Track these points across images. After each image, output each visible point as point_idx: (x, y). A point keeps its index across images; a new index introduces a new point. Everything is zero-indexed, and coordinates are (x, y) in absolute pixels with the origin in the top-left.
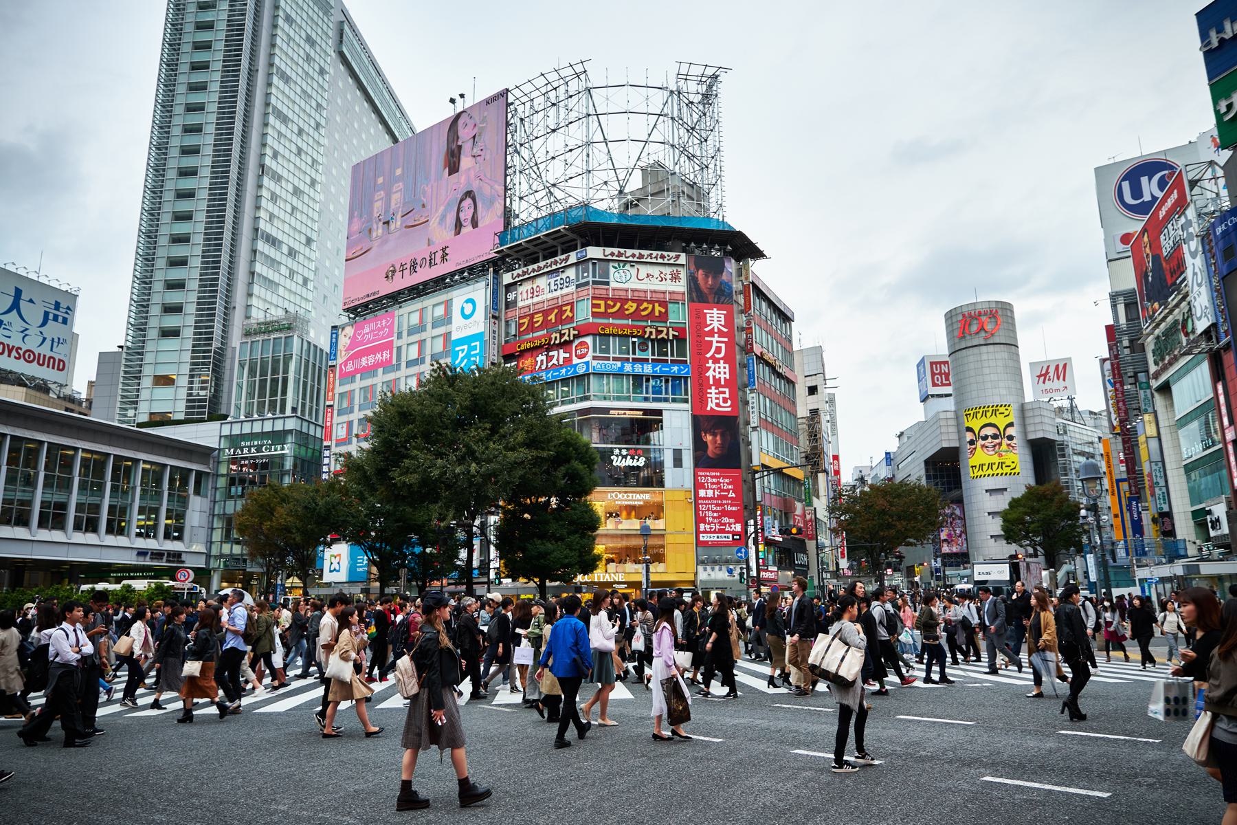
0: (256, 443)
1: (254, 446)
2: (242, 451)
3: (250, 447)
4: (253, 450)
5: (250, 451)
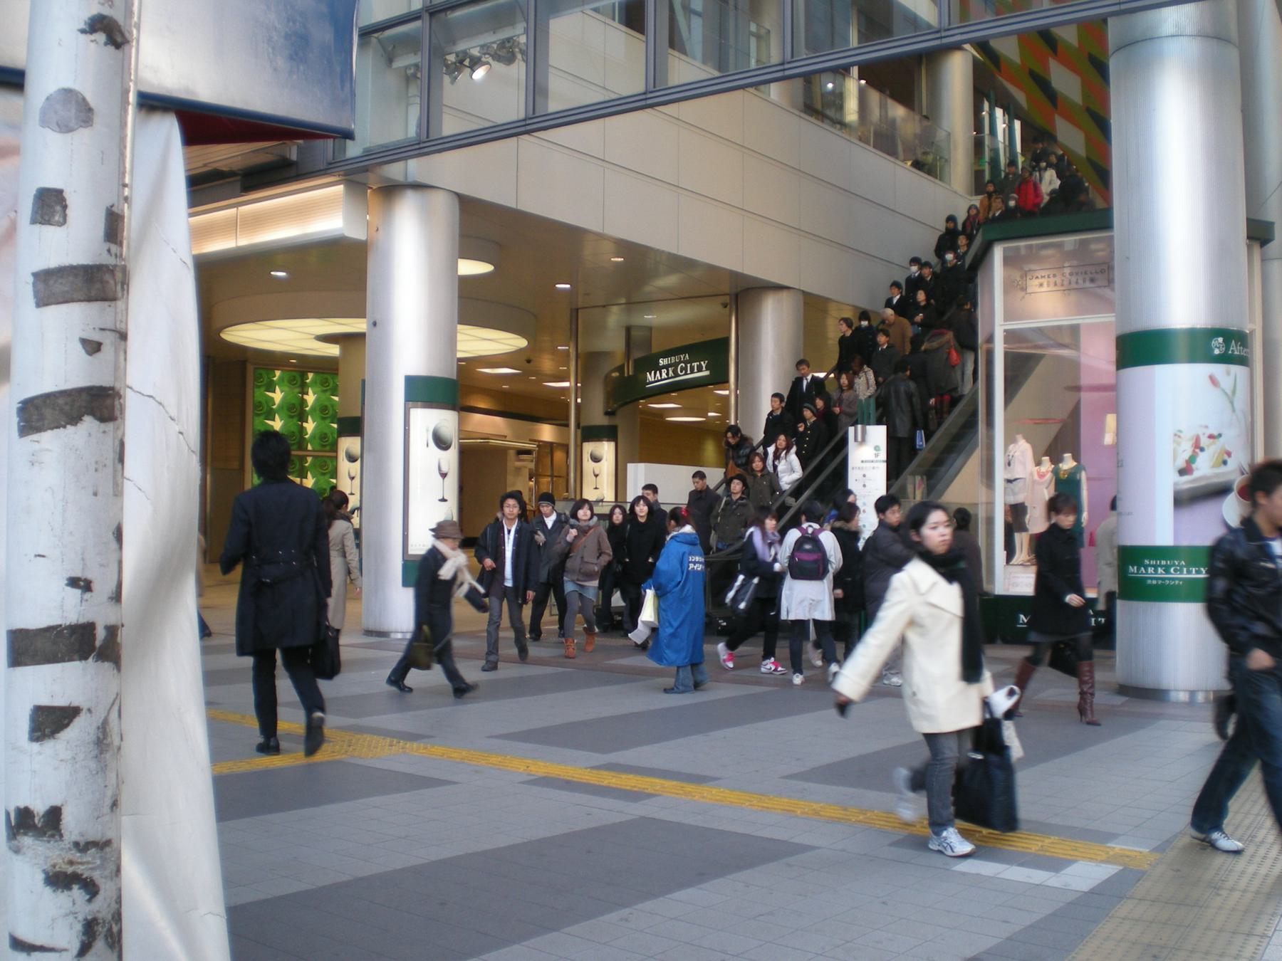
0: (1163, 563)
1: (1161, 566)
2: (1146, 570)
3: (1156, 567)
4: (1160, 570)
5: (1156, 571)
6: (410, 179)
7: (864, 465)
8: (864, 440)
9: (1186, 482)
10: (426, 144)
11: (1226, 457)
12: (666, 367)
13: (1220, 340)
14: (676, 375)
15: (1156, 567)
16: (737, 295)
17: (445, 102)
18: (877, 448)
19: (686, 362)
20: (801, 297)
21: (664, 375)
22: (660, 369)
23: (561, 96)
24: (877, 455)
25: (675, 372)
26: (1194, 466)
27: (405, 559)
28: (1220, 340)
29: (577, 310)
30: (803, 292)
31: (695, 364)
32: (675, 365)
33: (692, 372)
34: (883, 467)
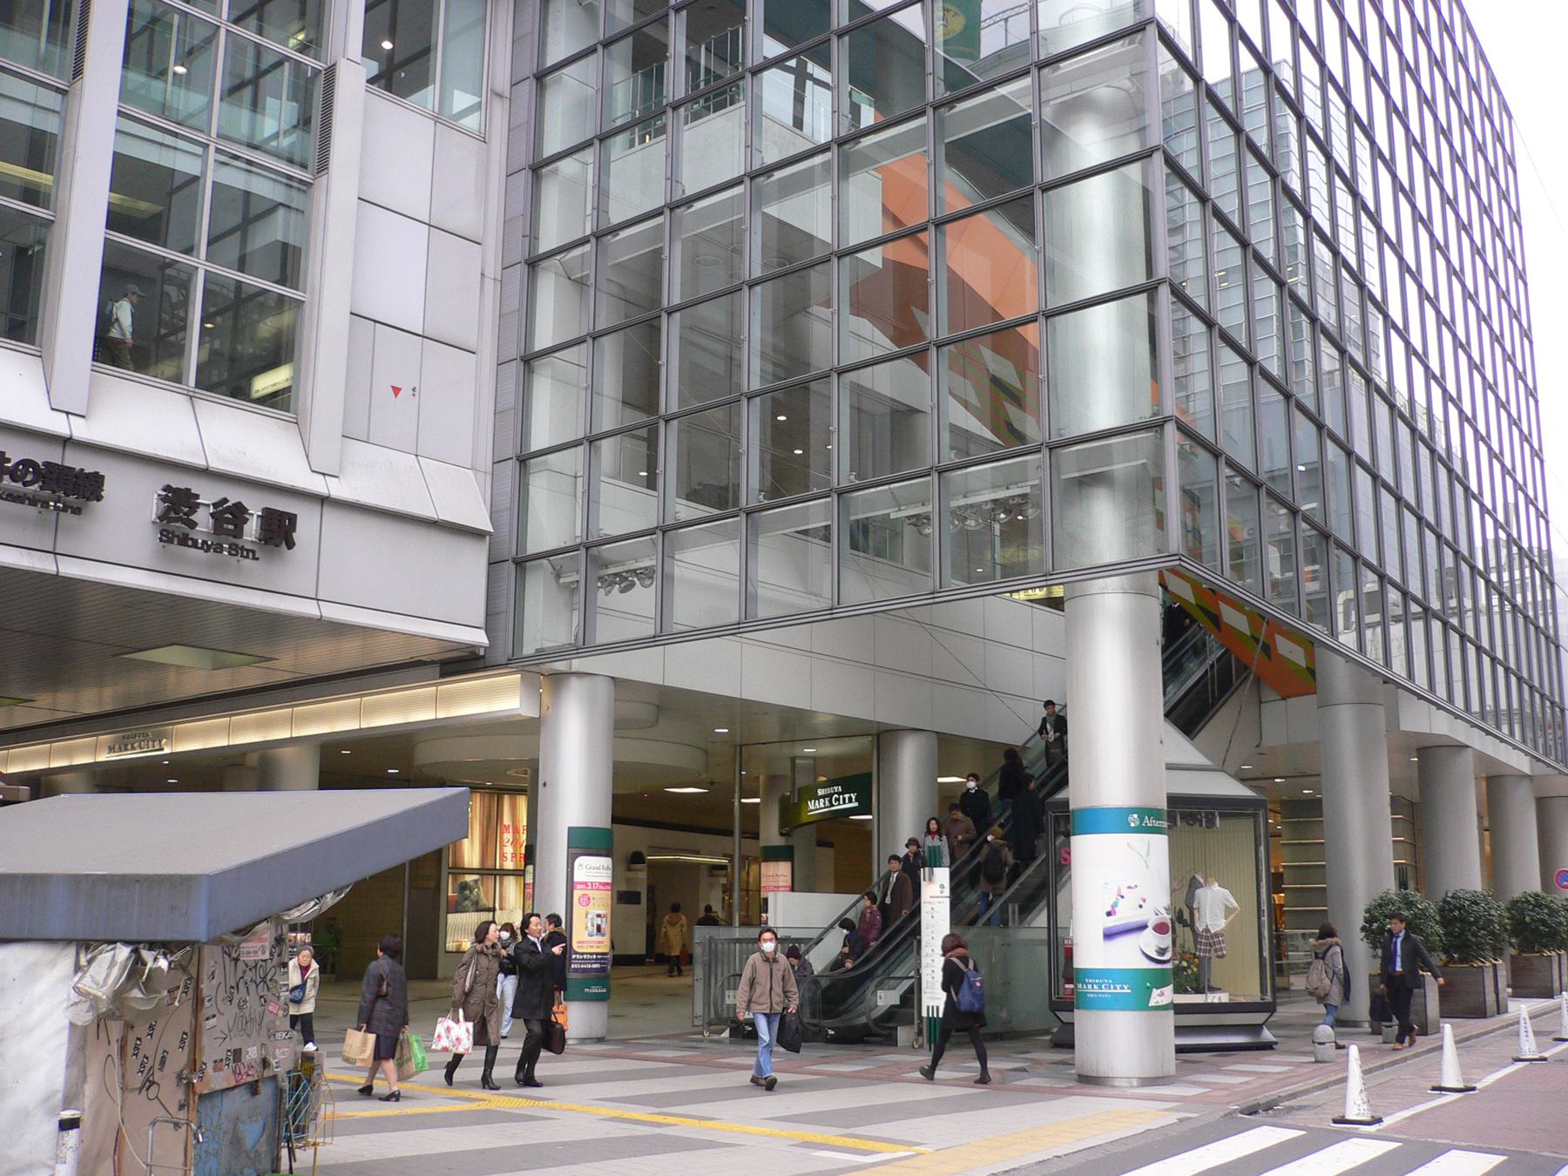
4: (1095, 987)
6: (573, 670)
7: (932, 900)
8: (930, 880)
9: (1112, 922)
10: (583, 646)
11: (1141, 903)
12: (823, 797)
13: (1135, 816)
14: (832, 805)
15: (1092, 984)
16: (878, 735)
17: (1003, 46)
18: (942, 886)
19: (839, 794)
20: (934, 738)
21: (822, 805)
22: (818, 798)
23: (685, 613)
24: (942, 892)
25: (830, 801)
26: (1116, 909)
27: (1233, 773)
28: (1135, 816)
29: (741, 746)
30: (937, 732)
31: (847, 796)
32: (830, 796)
33: (844, 803)
34: (947, 901)
